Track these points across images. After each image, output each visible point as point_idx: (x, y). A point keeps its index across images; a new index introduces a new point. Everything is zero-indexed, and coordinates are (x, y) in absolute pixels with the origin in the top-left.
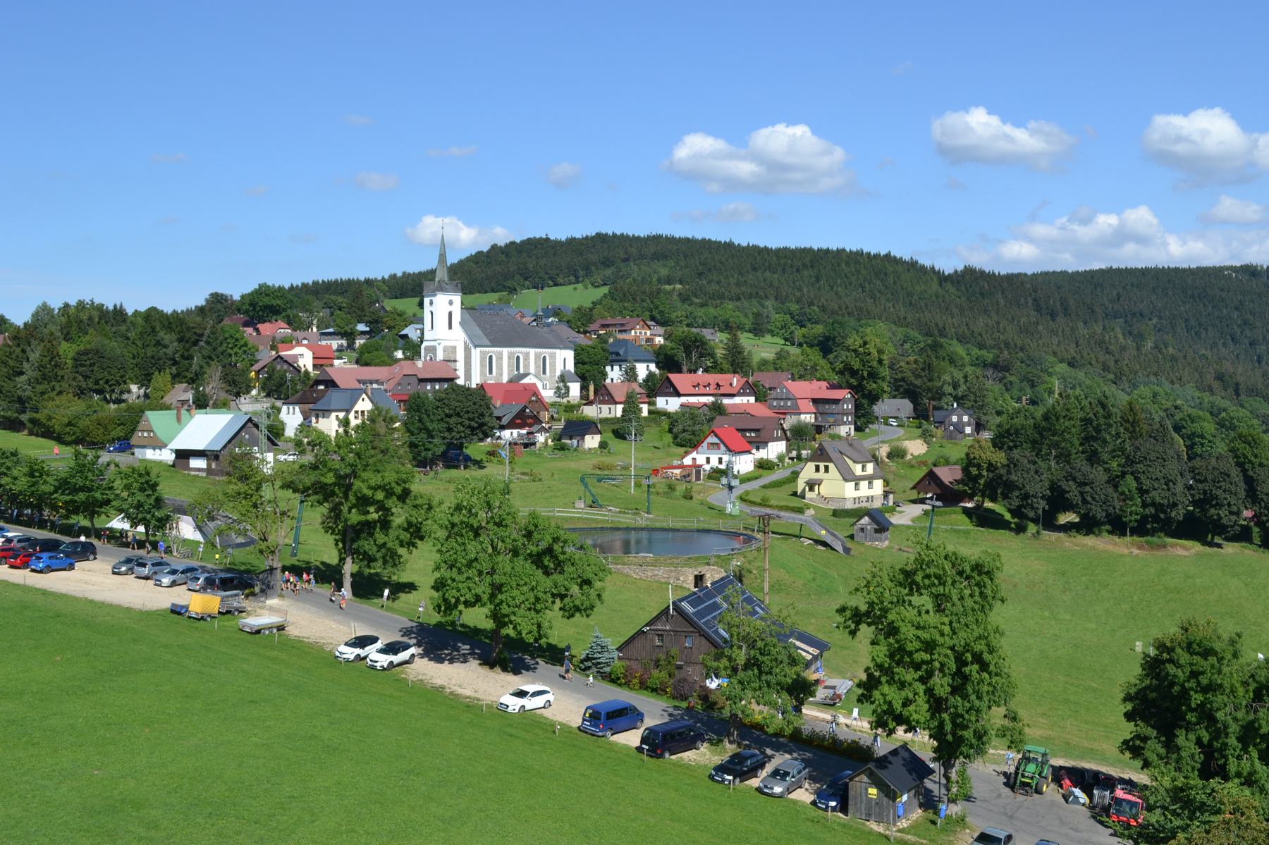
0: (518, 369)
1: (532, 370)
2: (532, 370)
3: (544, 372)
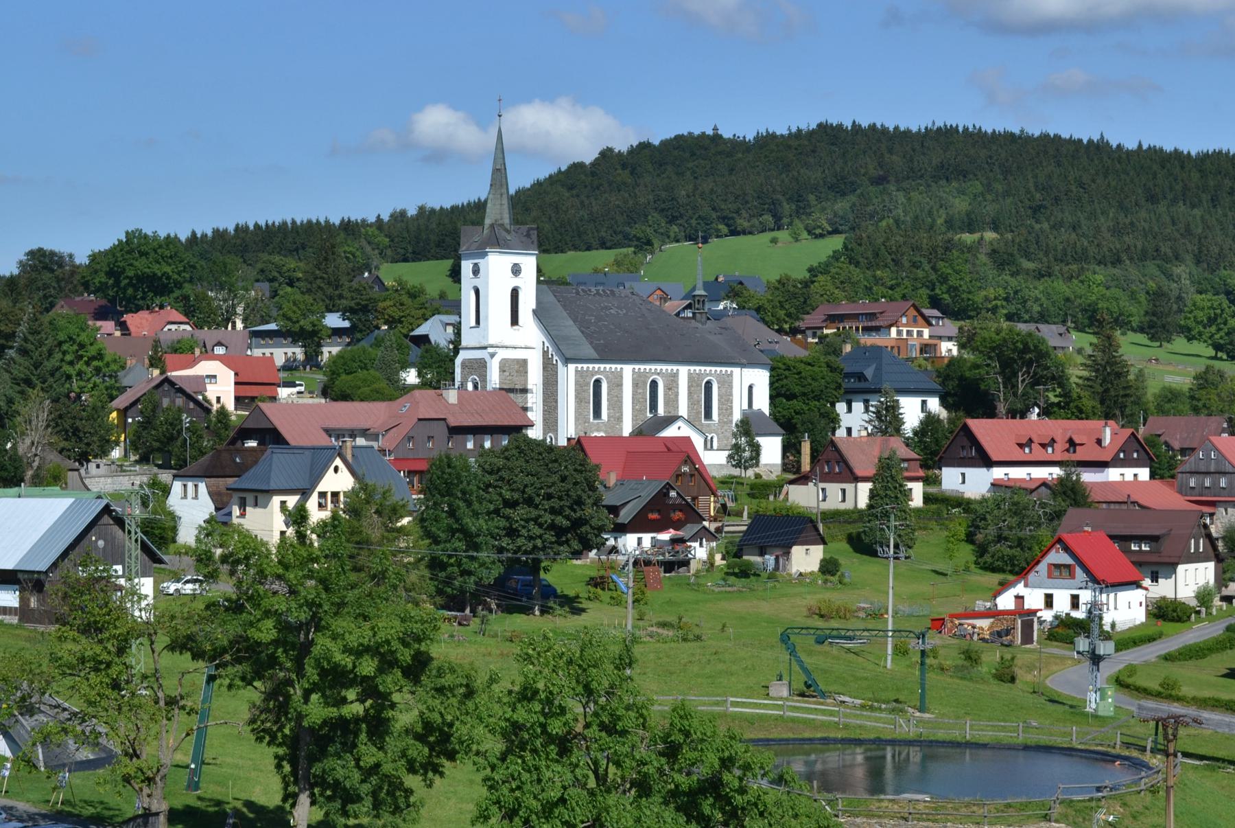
0: (654, 406)
1: (683, 410)
2: (683, 410)
3: (708, 415)
